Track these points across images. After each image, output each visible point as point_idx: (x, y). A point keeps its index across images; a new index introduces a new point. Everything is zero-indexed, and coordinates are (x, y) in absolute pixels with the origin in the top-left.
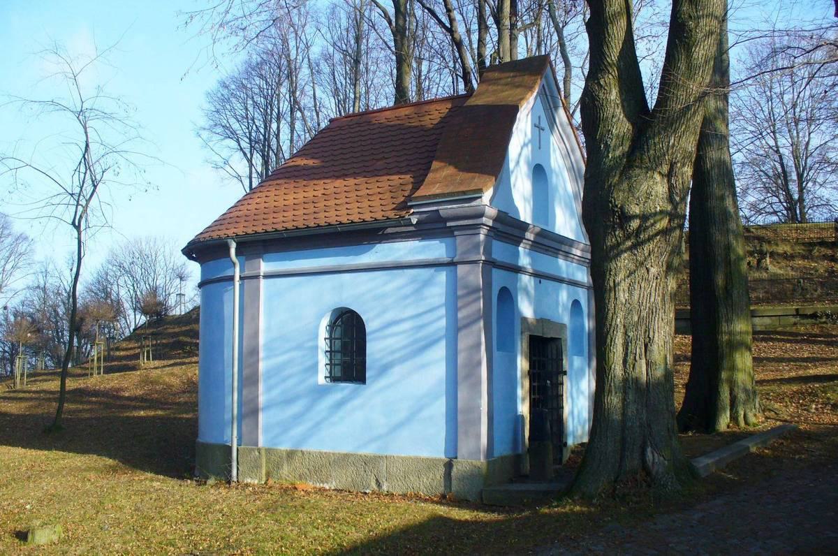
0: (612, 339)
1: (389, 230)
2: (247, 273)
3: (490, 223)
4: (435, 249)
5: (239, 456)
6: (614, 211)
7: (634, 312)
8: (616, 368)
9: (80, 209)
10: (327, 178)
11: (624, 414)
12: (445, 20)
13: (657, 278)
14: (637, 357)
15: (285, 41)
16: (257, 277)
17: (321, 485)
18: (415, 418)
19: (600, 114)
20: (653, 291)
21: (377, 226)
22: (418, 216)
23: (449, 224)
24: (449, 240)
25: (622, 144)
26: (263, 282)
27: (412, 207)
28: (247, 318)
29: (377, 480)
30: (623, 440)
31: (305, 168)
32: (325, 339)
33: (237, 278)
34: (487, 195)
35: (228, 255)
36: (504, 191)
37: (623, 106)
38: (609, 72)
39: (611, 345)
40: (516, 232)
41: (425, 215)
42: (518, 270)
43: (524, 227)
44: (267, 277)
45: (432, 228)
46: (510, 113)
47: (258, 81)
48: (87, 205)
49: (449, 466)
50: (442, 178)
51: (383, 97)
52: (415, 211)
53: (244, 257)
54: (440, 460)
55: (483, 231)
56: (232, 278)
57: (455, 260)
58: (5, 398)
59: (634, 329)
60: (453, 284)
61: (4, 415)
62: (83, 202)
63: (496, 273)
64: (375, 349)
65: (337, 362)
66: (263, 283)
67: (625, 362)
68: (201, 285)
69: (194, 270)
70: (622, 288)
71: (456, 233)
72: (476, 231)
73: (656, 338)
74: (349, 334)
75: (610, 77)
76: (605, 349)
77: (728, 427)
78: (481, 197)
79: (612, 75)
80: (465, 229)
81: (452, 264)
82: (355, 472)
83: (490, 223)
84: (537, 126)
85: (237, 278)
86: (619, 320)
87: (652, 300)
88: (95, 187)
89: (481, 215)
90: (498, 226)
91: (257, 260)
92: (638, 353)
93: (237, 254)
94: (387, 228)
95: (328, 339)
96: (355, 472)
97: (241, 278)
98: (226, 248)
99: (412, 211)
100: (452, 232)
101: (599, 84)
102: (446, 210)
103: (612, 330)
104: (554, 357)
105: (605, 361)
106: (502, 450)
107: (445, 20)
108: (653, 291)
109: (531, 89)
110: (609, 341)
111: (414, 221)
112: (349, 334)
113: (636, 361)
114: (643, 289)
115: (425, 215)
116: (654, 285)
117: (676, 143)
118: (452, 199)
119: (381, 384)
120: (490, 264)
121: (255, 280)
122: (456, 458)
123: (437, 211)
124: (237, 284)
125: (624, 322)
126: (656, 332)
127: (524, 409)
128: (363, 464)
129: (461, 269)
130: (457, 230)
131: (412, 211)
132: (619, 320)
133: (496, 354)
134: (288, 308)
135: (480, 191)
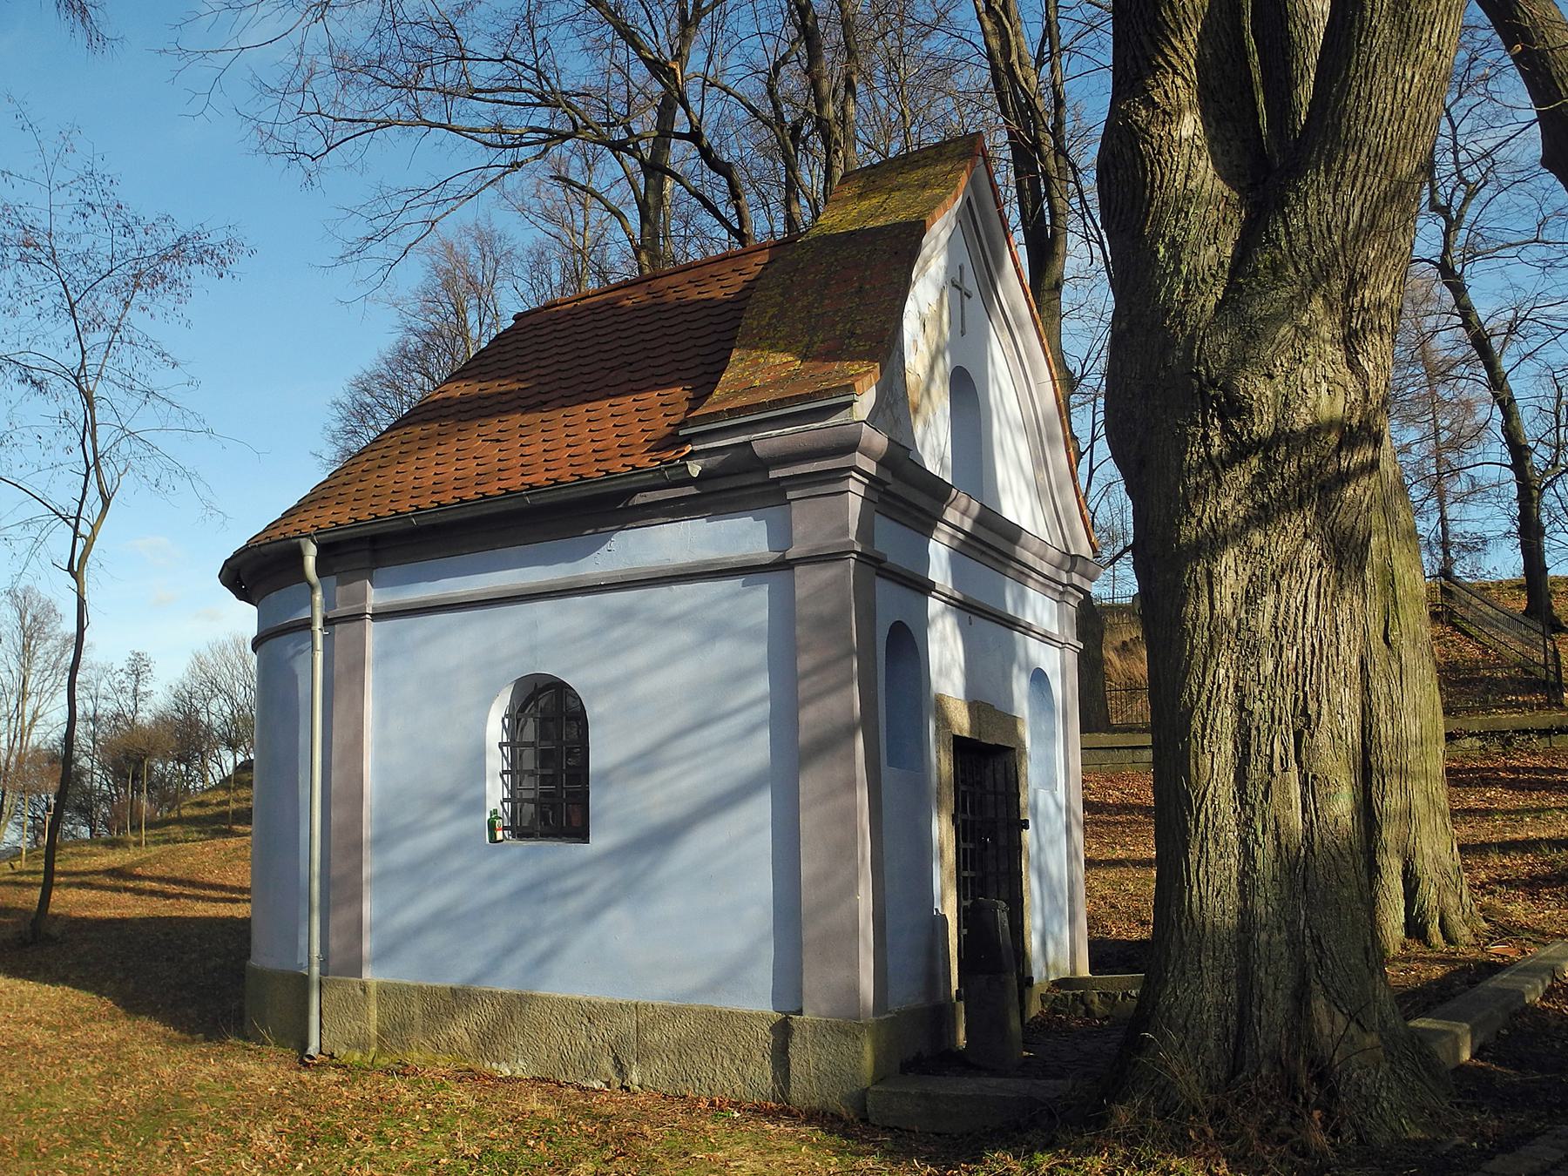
0: (1205, 720)
1: (639, 499)
2: (341, 610)
3: (871, 467)
4: (742, 536)
5: (1102, 753)
6: (1203, 394)
7: (1263, 650)
8: (1220, 792)
9: (80, 543)
10: (505, 377)
11: (1245, 913)
12: (729, 212)
13: (1320, 565)
14: (1276, 767)
15: (459, 312)
16: (359, 617)
17: (494, 1065)
18: (704, 922)
19: (1153, 174)
20: (1312, 600)
21: (613, 486)
22: (701, 461)
23: (773, 474)
24: (775, 512)
25: (1215, 238)
26: (370, 626)
27: (689, 439)
28: (339, 709)
29: (616, 1058)
30: (1246, 977)
31: (464, 400)
32: (501, 745)
33: (318, 624)
34: (865, 401)
35: (301, 576)
36: (895, 406)
37: (1213, 154)
38: (1175, 72)
39: (1203, 737)
40: (922, 500)
41: (720, 458)
42: (926, 588)
43: (938, 492)
44: (378, 616)
45: (734, 487)
46: (904, 244)
47: (419, 379)
48: (94, 534)
49: (783, 1031)
50: (756, 371)
51: (619, 260)
52: (697, 448)
53: (334, 578)
54: (762, 1017)
55: (855, 489)
56: (307, 625)
57: (792, 554)
58: (6, 883)
59: (1265, 695)
60: (784, 612)
61: (5, 911)
62: (84, 529)
63: (883, 588)
64: (605, 750)
65: (526, 795)
66: (372, 629)
67: (1241, 777)
68: (257, 644)
69: (243, 619)
70: (1229, 592)
71: (790, 495)
72: (840, 487)
73: (1325, 718)
74: (552, 725)
75: (1179, 81)
76: (1187, 746)
77: (1404, 947)
78: (850, 404)
79: (1184, 79)
80: (814, 484)
81: (783, 565)
82: (566, 1038)
83: (871, 467)
84: (955, 283)
85: (318, 624)
86: (1222, 671)
87: (1310, 619)
88: (106, 503)
89: (851, 447)
90: (887, 477)
91: (356, 585)
92: (1276, 755)
93: (321, 569)
94: (633, 492)
95: (506, 744)
96: (566, 1038)
97: (327, 622)
98: (299, 556)
99: (689, 448)
100: (783, 492)
101: (1151, 104)
102: (768, 441)
103: (1204, 698)
104: (1001, 788)
105: (1188, 776)
106: (906, 996)
107: (729, 212)
108: (1312, 600)
109: (951, 187)
110: (1196, 724)
111: (695, 469)
112: (552, 725)
113: (1273, 775)
114: (1284, 594)
115: (720, 458)
116: (1314, 582)
117: (1364, 223)
118: (779, 413)
119: (625, 808)
120: (872, 563)
121: (357, 623)
122: (800, 1012)
123: (748, 443)
124: (319, 636)
125: (1237, 678)
126: (1324, 701)
127: (948, 906)
128: (586, 1021)
129: (807, 580)
130: (792, 488)
131: (689, 448)
132: (1222, 671)
133: (886, 771)
134: (427, 698)
135: (849, 389)
